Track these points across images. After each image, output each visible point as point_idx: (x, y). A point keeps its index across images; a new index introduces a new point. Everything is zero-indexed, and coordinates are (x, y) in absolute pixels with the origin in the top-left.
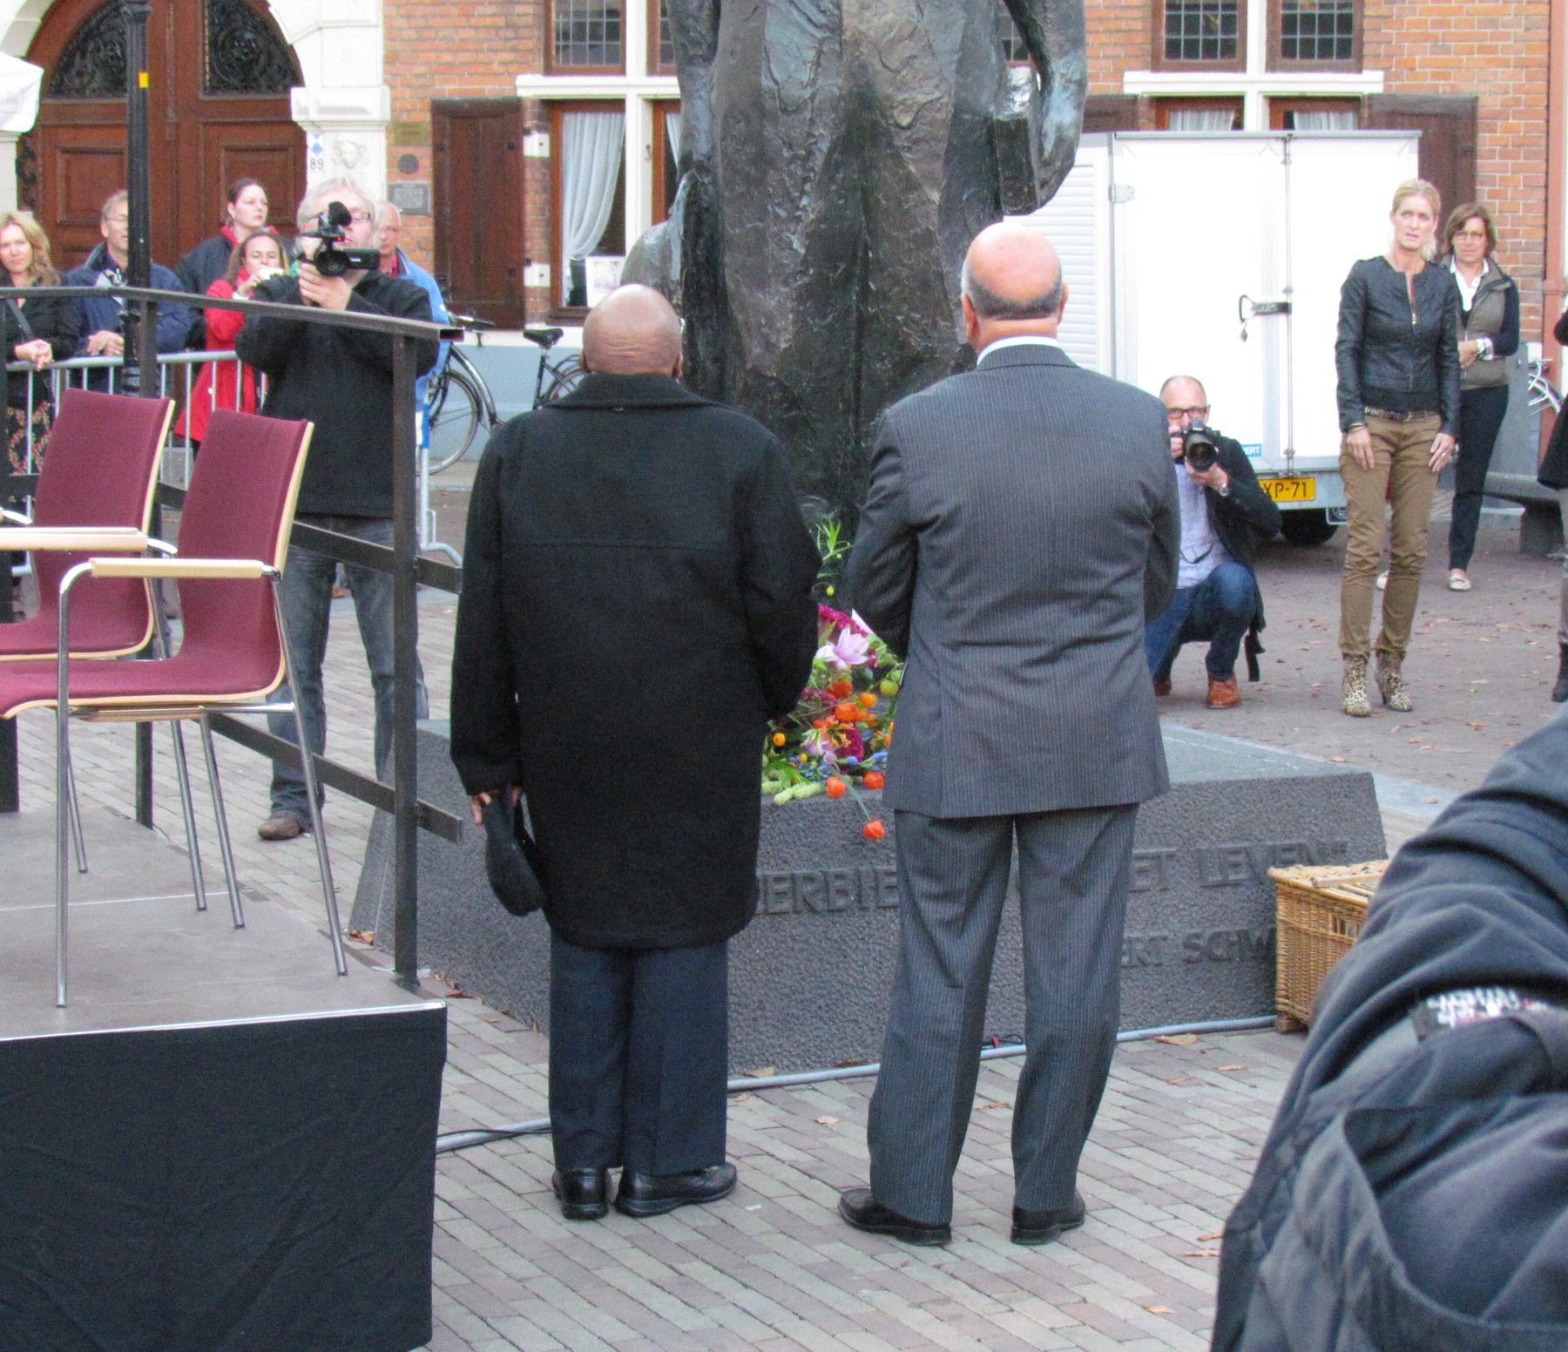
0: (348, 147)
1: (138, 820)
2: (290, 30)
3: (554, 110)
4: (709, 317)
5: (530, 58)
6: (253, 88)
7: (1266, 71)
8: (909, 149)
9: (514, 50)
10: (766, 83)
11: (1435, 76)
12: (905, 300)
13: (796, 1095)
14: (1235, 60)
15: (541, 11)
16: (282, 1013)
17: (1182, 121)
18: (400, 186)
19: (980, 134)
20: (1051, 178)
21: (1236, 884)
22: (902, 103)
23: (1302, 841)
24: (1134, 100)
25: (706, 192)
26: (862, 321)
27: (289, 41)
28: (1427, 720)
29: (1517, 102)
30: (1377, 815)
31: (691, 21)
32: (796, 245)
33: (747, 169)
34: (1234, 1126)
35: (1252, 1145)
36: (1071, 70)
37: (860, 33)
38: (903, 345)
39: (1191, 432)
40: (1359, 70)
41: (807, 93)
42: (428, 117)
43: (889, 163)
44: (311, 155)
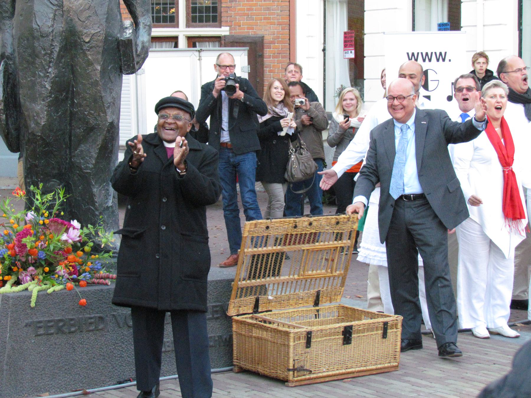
7: (186, 27)
8: (89, 50)
10: (35, 26)
11: (248, 29)
12: (88, 106)
19: (114, 45)
20: (140, 60)
22: (85, 33)
25: (11, 67)
26: (72, 114)
29: (278, 38)
31: (4, 3)
32: (47, 86)
33: (28, 58)
36: (146, 21)
37: (70, 7)
38: (87, 123)
40: (220, 27)
41: (50, 30)
43: (82, 55)
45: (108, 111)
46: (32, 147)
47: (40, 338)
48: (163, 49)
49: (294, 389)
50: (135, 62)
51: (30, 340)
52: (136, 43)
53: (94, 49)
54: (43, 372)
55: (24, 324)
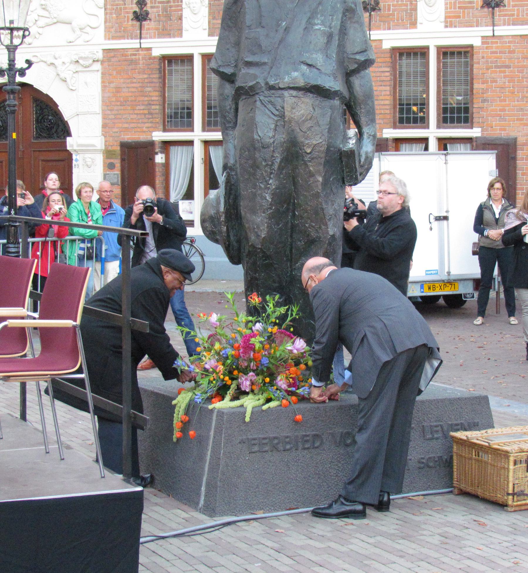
0: (88, 160)
1: (21, 418)
2: (66, 116)
3: (167, 145)
4: (235, 225)
5: (158, 125)
6: (52, 137)
8: (310, 161)
9: (152, 122)
10: (256, 137)
11: (501, 130)
12: (309, 218)
13: (272, 521)
14: (425, 125)
15: (161, 107)
16: (81, 492)
17: (404, 147)
18: (108, 174)
19: (337, 156)
21: (437, 439)
22: (307, 144)
23: (462, 421)
24: (387, 140)
26: (293, 227)
27: (66, 120)
28: (504, 374)
30: (490, 411)
31: (227, 114)
34: (440, 531)
35: (446, 538)
37: (292, 118)
39: (147, 202)
40: (472, 128)
42: (119, 148)
43: (303, 167)
44: (74, 162)
45: (329, 223)
46: (252, 260)
47: (254, 455)
48: (413, 152)
49: (513, 514)
50: (358, 174)
51: (244, 457)
52: (359, 153)
53: (316, 160)
54: (257, 489)
55: (238, 441)
